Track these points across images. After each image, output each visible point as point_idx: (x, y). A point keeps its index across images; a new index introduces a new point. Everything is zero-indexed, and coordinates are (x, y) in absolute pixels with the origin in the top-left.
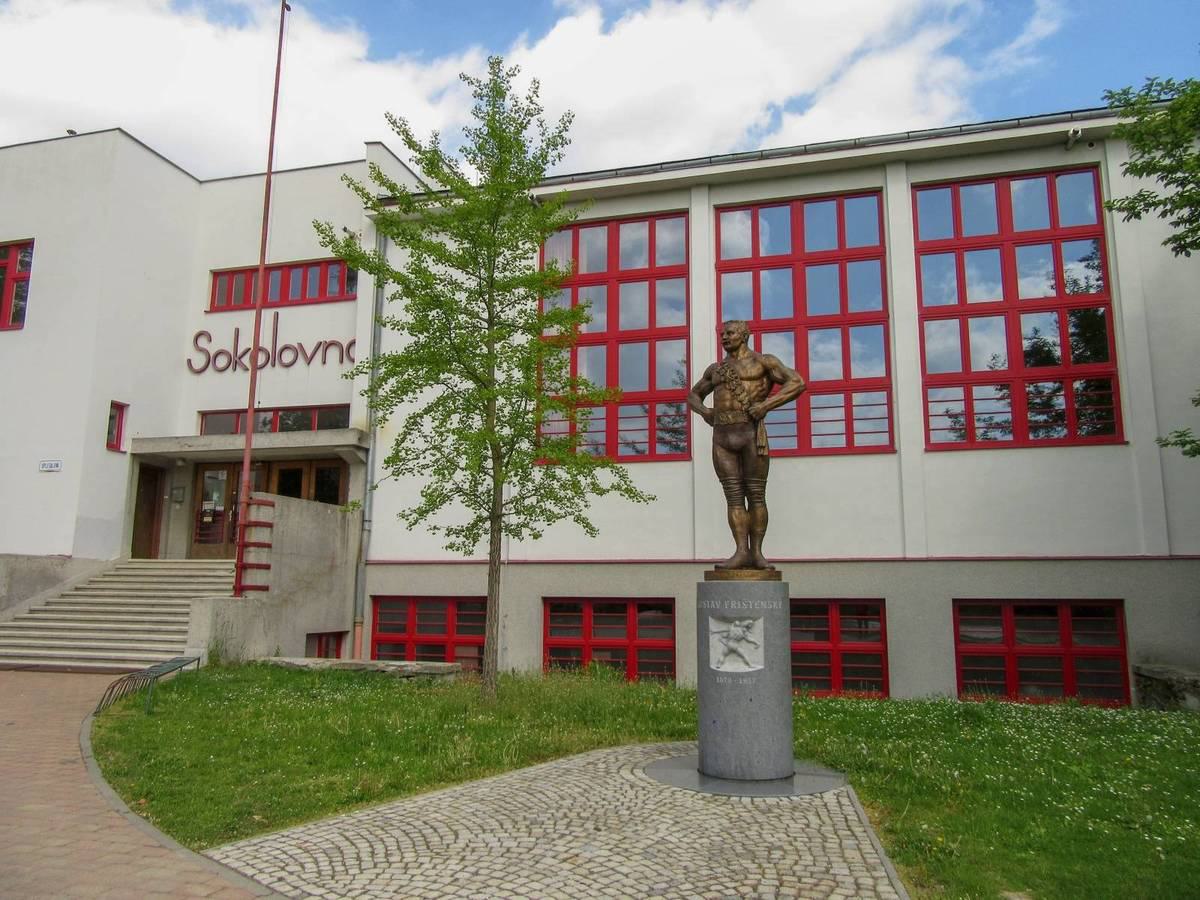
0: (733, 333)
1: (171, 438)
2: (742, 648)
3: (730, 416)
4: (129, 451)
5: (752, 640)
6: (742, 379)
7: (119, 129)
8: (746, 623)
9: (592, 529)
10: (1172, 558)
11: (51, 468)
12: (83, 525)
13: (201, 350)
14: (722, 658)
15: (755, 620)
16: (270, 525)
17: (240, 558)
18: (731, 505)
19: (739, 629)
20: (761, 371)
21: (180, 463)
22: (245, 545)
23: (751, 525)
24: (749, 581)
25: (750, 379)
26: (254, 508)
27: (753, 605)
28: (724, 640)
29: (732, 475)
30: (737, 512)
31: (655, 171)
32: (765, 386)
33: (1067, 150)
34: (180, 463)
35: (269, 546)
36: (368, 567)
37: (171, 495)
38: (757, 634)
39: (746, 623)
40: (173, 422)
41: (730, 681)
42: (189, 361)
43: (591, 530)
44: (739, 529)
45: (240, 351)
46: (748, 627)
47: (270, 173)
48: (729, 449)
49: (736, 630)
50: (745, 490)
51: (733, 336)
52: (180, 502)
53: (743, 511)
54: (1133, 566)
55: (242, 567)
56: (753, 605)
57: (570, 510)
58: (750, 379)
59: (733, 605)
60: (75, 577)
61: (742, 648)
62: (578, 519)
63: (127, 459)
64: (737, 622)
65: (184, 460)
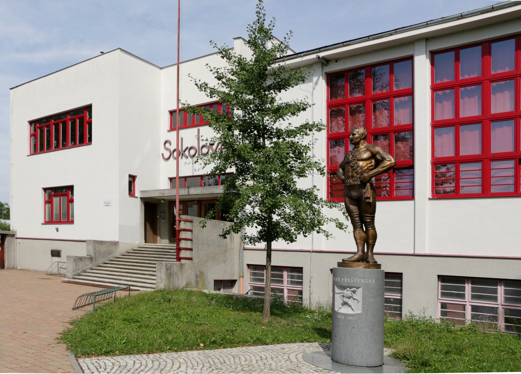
1: (155, 190)
2: (350, 301)
4: (139, 197)
5: (356, 298)
7: (120, 48)
8: (352, 289)
11: (107, 204)
12: (122, 229)
13: (167, 149)
14: (340, 306)
15: (358, 288)
16: (191, 231)
17: (178, 245)
18: (355, 228)
19: (349, 292)
20: (370, 155)
21: (162, 202)
22: (180, 240)
23: (368, 238)
24: (360, 268)
26: (182, 223)
27: (357, 281)
28: (342, 298)
31: (391, 35)
32: (372, 164)
34: (162, 202)
35: (191, 240)
36: (245, 251)
37: (160, 216)
38: (359, 294)
39: (352, 289)
40: (158, 181)
41: (343, 317)
42: (163, 154)
44: (358, 241)
45: (184, 149)
46: (354, 292)
47: (178, 64)
49: (348, 292)
50: (362, 221)
52: (164, 219)
55: (179, 250)
56: (357, 281)
59: (346, 280)
60: (122, 249)
61: (350, 301)
63: (138, 201)
64: (348, 289)
65: (164, 200)
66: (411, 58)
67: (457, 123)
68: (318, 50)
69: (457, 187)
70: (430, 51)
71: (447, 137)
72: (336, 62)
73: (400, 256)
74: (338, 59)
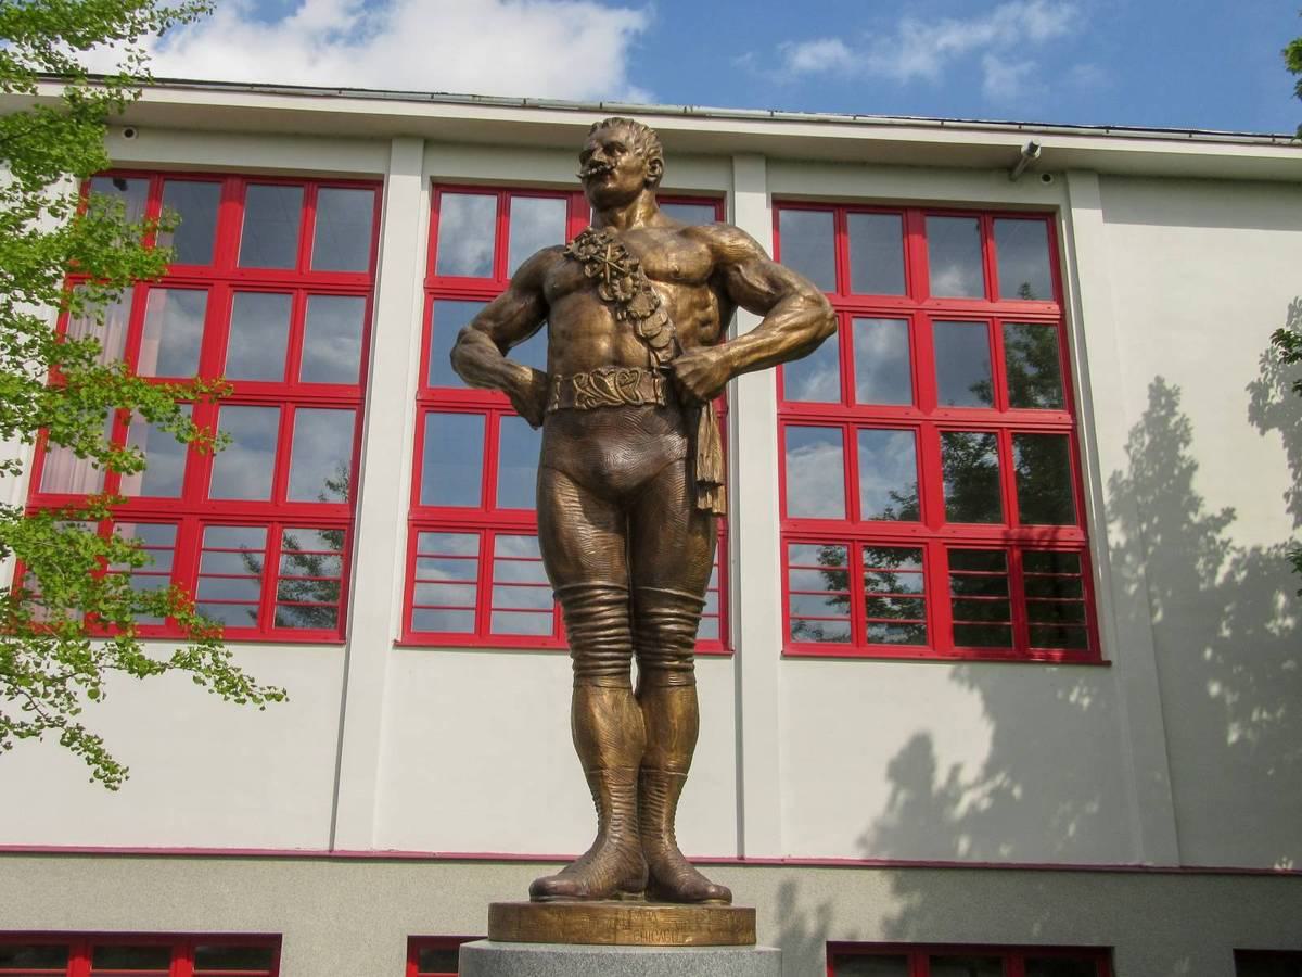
0: (623, 150)
3: (609, 382)
6: (652, 275)
9: (111, 768)
10: (1186, 872)
20: (707, 261)
25: (673, 277)
29: (598, 575)
30: (606, 698)
33: (1012, 180)
43: (108, 772)
44: (610, 757)
48: (601, 491)
51: (624, 159)
53: (624, 697)
54: (992, 880)
57: (53, 713)
58: (673, 277)
62: (73, 738)
66: (375, 184)
67: (289, 396)
68: (248, 88)
69: (483, 608)
70: (431, 177)
71: (823, 460)
72: (129, 134)
73: (279, 864)
74: (136, 127)
